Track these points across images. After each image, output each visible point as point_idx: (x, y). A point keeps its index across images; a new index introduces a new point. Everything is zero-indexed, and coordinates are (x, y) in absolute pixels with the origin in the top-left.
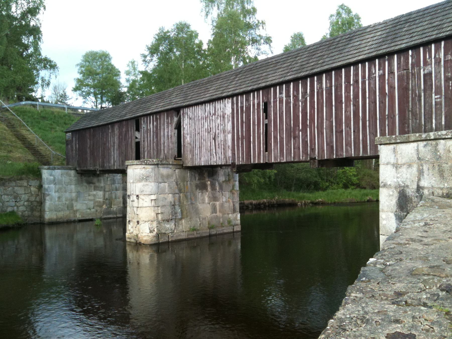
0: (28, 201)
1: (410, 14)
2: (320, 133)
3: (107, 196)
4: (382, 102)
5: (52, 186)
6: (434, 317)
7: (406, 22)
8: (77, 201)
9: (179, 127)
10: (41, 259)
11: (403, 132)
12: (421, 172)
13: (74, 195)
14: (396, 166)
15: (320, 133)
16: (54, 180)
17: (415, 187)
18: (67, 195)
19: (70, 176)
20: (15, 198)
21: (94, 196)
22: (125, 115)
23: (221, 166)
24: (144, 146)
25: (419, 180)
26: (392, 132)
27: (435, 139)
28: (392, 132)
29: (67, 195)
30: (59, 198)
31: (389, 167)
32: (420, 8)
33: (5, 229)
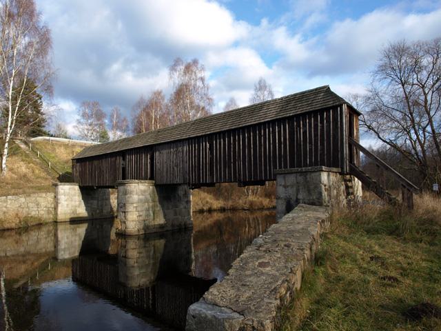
0: (46, 207)
1: (295, 95)
2: (244, 164)
3: (100, 204)
4: (280, 147)
5: (63, 196)
6: (279, 256)
7: (294, 99)
8: (79, 207)
9: (152, 159)
10: (56, 246)
11: (292, 166)
12: (298, 191)
13: (77, 203)
14: (285, 187)
15: (244, 164)
16: (64, 193)
17: (295, 198)
18: (73, 203)
19: (75, 190)
20: (38, 205)
21: (92, 204)
22: (116, 148)
23: (180, 184)
24: (128, 170)
25: (297, 195)
26: (285, 167)
27: (305, 172)
28: (286, 167)
29: (73, 203)
30: (67, 205)
31: (281, 187)
32: (304, 90)
33: (4, 230)
